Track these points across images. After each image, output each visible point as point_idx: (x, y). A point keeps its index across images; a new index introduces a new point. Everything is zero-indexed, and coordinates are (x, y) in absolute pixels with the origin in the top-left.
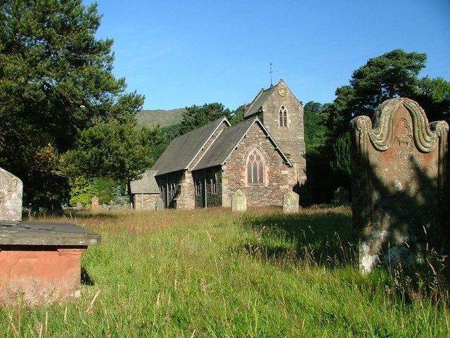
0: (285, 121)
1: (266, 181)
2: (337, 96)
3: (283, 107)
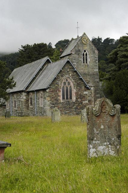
0: (86, 60)
1: (74, 98)
3: (85, 51)
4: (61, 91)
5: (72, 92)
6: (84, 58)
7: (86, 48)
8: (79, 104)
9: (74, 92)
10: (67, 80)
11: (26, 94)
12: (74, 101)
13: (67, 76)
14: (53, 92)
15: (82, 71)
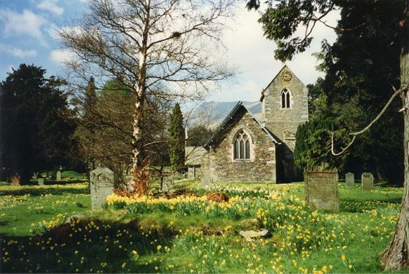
1: (252, 157)
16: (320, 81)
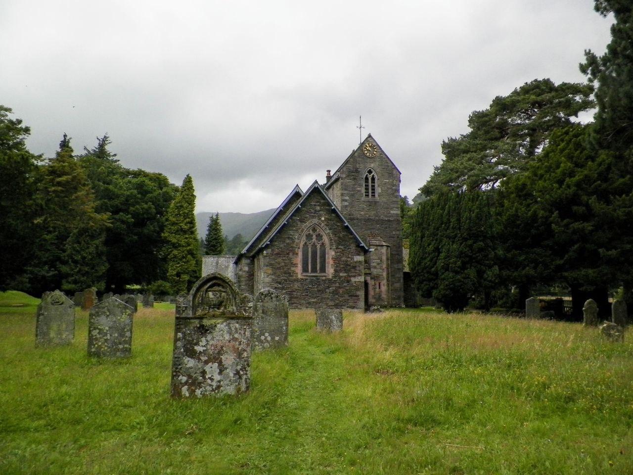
0: (373, 189)
1: (330, 271)
2: (582, 79)
3: (370, 172)
4: (300, 254)
5: (327, 256)
6: (367, 186)
7: (372, 165)
8: (342, 282)
9: (331, 257)
10: (314, 230)
11: (248, 261)
12: (330, 277)
13: (315, 221)
14: (280, 257)
15: (362, 213)
16: (615, 30)
